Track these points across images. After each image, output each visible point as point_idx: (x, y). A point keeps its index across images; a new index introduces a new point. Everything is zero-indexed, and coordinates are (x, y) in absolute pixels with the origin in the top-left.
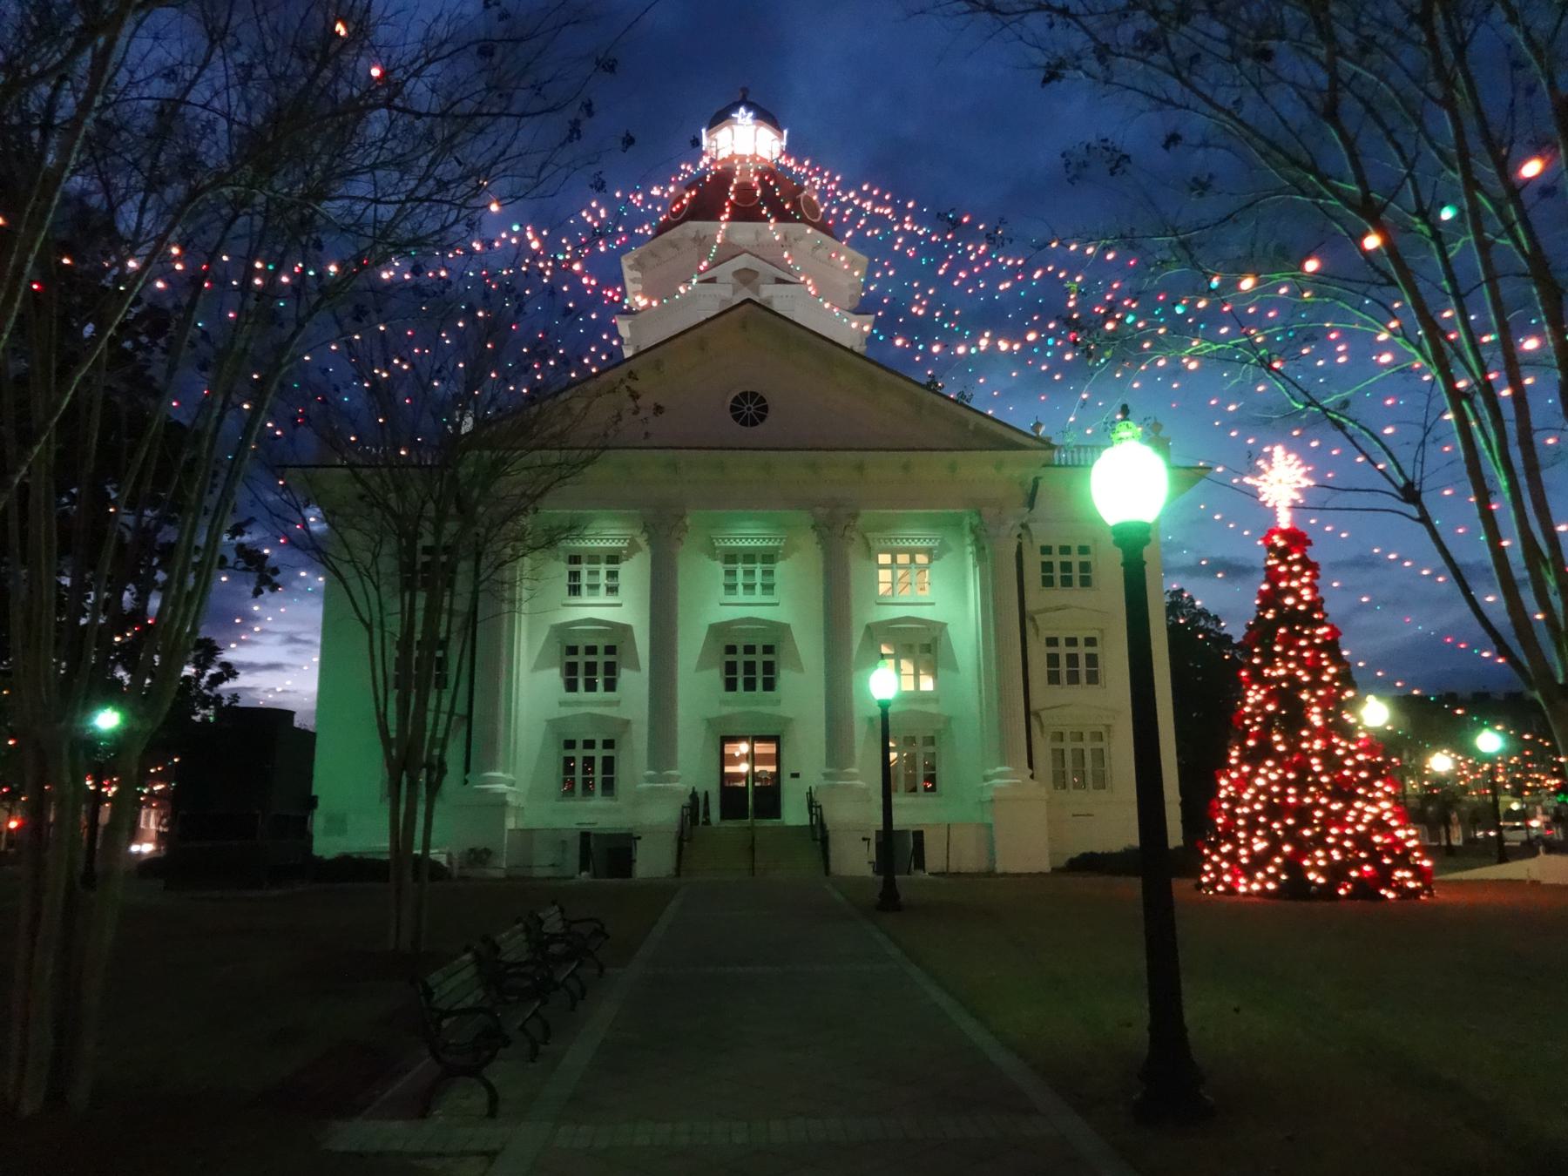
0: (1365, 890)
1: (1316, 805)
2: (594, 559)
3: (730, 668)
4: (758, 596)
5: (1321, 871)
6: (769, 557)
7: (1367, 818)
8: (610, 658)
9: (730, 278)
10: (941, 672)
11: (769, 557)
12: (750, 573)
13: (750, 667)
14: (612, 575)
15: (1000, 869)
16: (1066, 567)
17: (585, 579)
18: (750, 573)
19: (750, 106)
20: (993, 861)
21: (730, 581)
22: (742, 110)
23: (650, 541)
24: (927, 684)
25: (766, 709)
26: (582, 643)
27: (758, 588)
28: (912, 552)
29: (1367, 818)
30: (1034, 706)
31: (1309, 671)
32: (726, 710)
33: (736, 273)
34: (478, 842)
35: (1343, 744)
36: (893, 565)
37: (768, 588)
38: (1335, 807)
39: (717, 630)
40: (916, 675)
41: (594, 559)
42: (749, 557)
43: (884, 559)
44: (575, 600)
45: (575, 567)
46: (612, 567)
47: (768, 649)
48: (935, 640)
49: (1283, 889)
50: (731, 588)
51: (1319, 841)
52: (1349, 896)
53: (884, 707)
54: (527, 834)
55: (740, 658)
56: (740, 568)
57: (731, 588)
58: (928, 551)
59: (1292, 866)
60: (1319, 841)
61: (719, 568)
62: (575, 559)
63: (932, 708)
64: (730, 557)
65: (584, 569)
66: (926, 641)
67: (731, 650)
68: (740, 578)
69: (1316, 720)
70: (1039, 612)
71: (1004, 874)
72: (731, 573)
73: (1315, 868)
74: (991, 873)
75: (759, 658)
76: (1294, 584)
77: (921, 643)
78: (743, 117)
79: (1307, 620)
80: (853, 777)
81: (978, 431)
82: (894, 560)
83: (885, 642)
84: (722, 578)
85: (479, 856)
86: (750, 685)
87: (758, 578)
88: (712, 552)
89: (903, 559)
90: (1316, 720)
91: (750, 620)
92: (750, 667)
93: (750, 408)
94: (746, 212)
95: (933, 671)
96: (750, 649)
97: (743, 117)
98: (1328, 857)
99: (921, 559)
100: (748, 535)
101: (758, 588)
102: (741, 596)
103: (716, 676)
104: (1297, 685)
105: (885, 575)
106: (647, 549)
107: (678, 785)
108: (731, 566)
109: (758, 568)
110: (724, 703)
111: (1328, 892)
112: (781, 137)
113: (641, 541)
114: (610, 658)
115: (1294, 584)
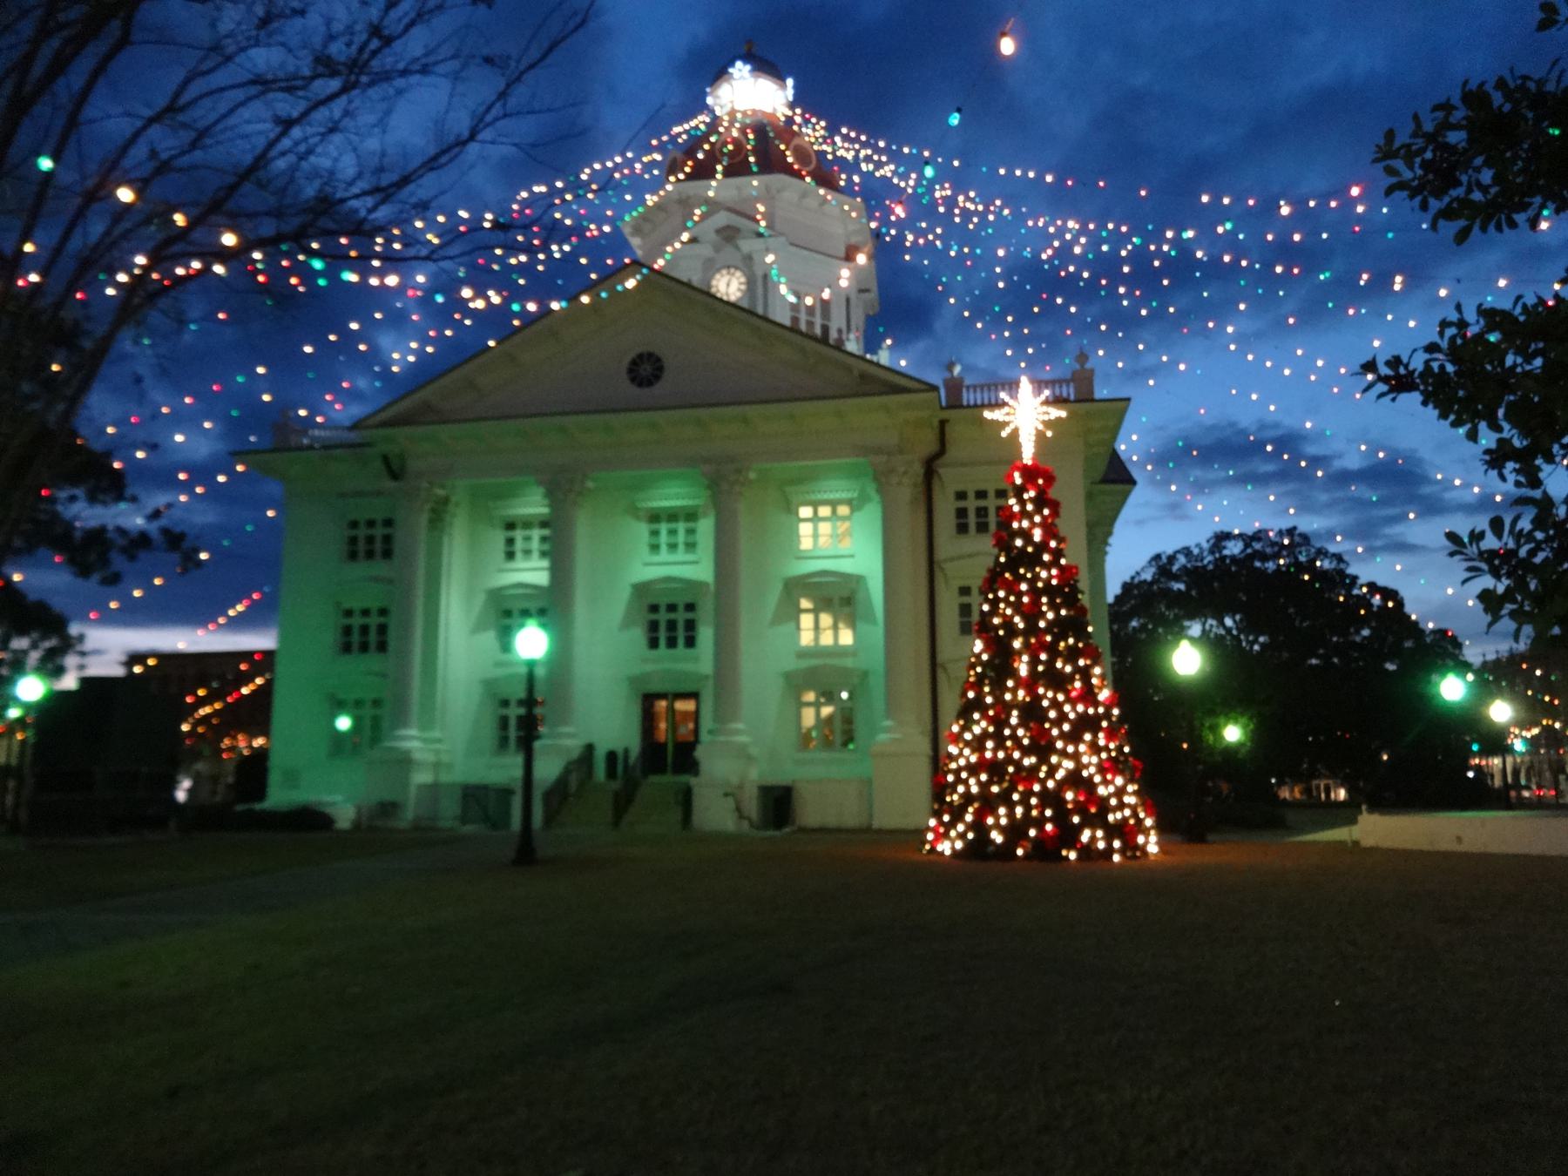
0: (1046, 851)
1: (1009, 760)
2: (527, 524)
3: (653, 627)
4: (681, 555)
5: (1002, 830)
6: (691, 515)
7: (1060, 774)
8: (690, 615)
9: (713, 236)
10: (859, 625)
11: (691, 515)
12: (673, 532)
13: (672, 625)
14: (691, 532)
15: (876, 824)
16: (982, 512)
17: (519, 545)
18: (673, 532)
19: (747, 58)
20: (871, 816)
21: (654, 541)
22: (739, 64)
23: (880, 491)
24: (846, 638)
25: (688, 667)
26: (663, 601)
27: (681, 547)
28: (834, 504)
29: (1060, 774)
30: (941, 658)
31: (1025, 618)
32: (649, 668)
33: (718, 231)
34: (387, 796)
35: (1050, 694)
36: (816, 519)
37: (691, 546)
38: (1027, 762)
39: (641, 589)
40: (835, 628)
41: (527, 524)
42: (672, 516)
43: (805, 512)
44: (656, 559)
45: (510, 534)
46: (691, 525)
47: (690, 607)
48: (854, 592)
49: (969, 845)
50: (655, 548)
51: (1005, 798)
52: (1026, 856)
53: (531, 665)
54: (434, 789)
55: (663, 617)
56: (664, 528)
57: (655, 548)
58: (849, 502)
59: (979, 826)
60: (1005, 798)
61: (643, 529)
62: (511, 526)
63: (849, 663)
64: (655, 517)
65: (518, 534)
66: (845, 594)
67: (654, 608)
68: (664, 538)
69: (1023, 670)
70: (946, 561)
71: (823, 830)
72: (655, 533)
73: (997, 826)
74: (868, 830)
75: (681, 617)
76: (1025, 524)
77: (838, 596)
78: (741, 69)
79: (1033, 561)
80: (737, 732)
81: (864, 377)
82: (834, 512)
83: (807, 596)
84: (500, 545)
85: (388, 809)
86: (672, 643)
87: (681, 538)
88: (634, 512)
89: (825, 511)
90: (1023, 670)
91: (669, 579)
92: (672, 625)
93: (646, 370)
94: (737, 168)
95: (852, 624)
96: (672, 608)
97: (741, 69)
98: (1011, 815)
99: (843, 510)
100: (672, 495)
101: (664, 548)
102: (664, 555)
103: (638, 635)
104: (1012, 631)
105: (805, 529)
106: (876, 498)
107: (569, 742)
108: (655, 526)
109: (681, 527)
110: (645, 661)
111: (1006, 851)
112: (784, 87)
113: (871, 489)
114: (690, 615)
115: (1025, 524)
